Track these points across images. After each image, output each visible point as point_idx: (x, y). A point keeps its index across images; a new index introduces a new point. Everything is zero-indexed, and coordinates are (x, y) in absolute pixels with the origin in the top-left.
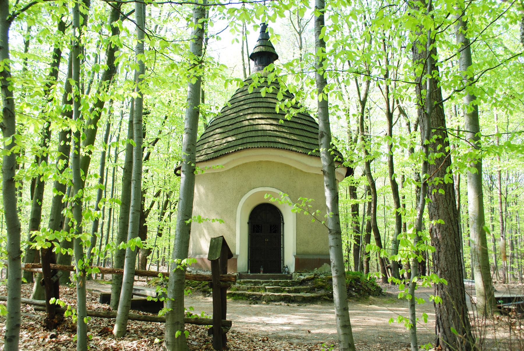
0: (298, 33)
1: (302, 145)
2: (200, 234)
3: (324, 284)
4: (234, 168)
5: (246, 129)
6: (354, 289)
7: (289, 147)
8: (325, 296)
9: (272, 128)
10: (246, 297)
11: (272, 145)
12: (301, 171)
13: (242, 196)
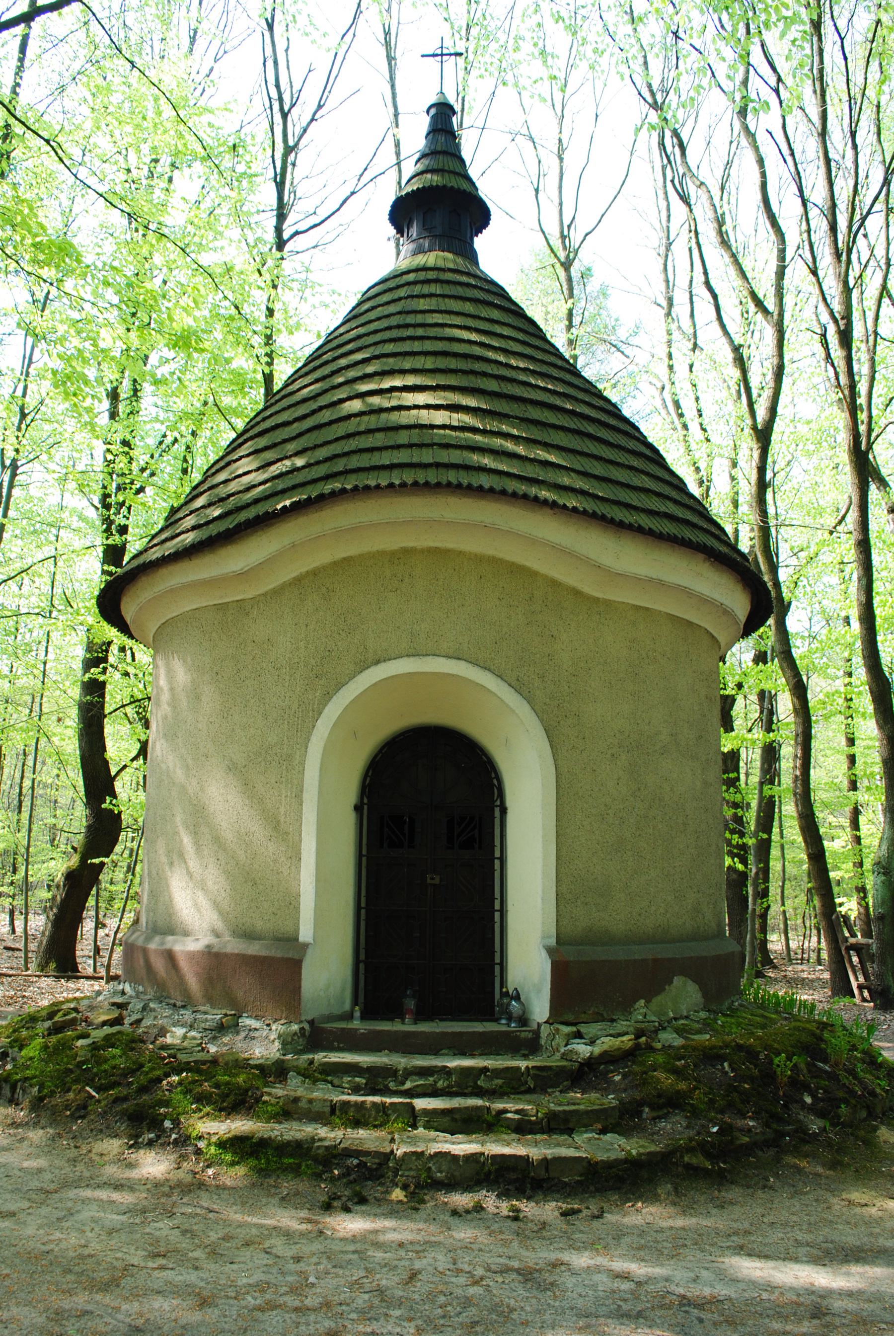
0: (562, 264)
1: (580, 483)
2: (169, 852)
3: (682, 1086)
4: (298, 581)
5: (351, 426)
6: (808, 1100)
7: (523, 488)
8: (690, 1150)
9: (456, 419)
10: (316, 1159)
11: (452, 476)
12: (577, 593)
13: (328, 696)
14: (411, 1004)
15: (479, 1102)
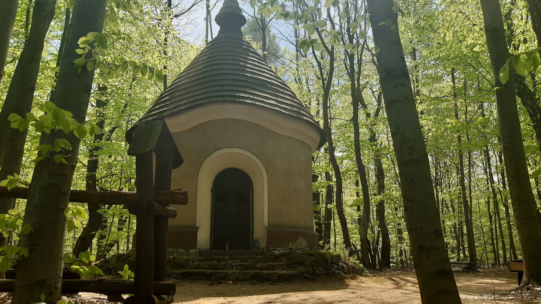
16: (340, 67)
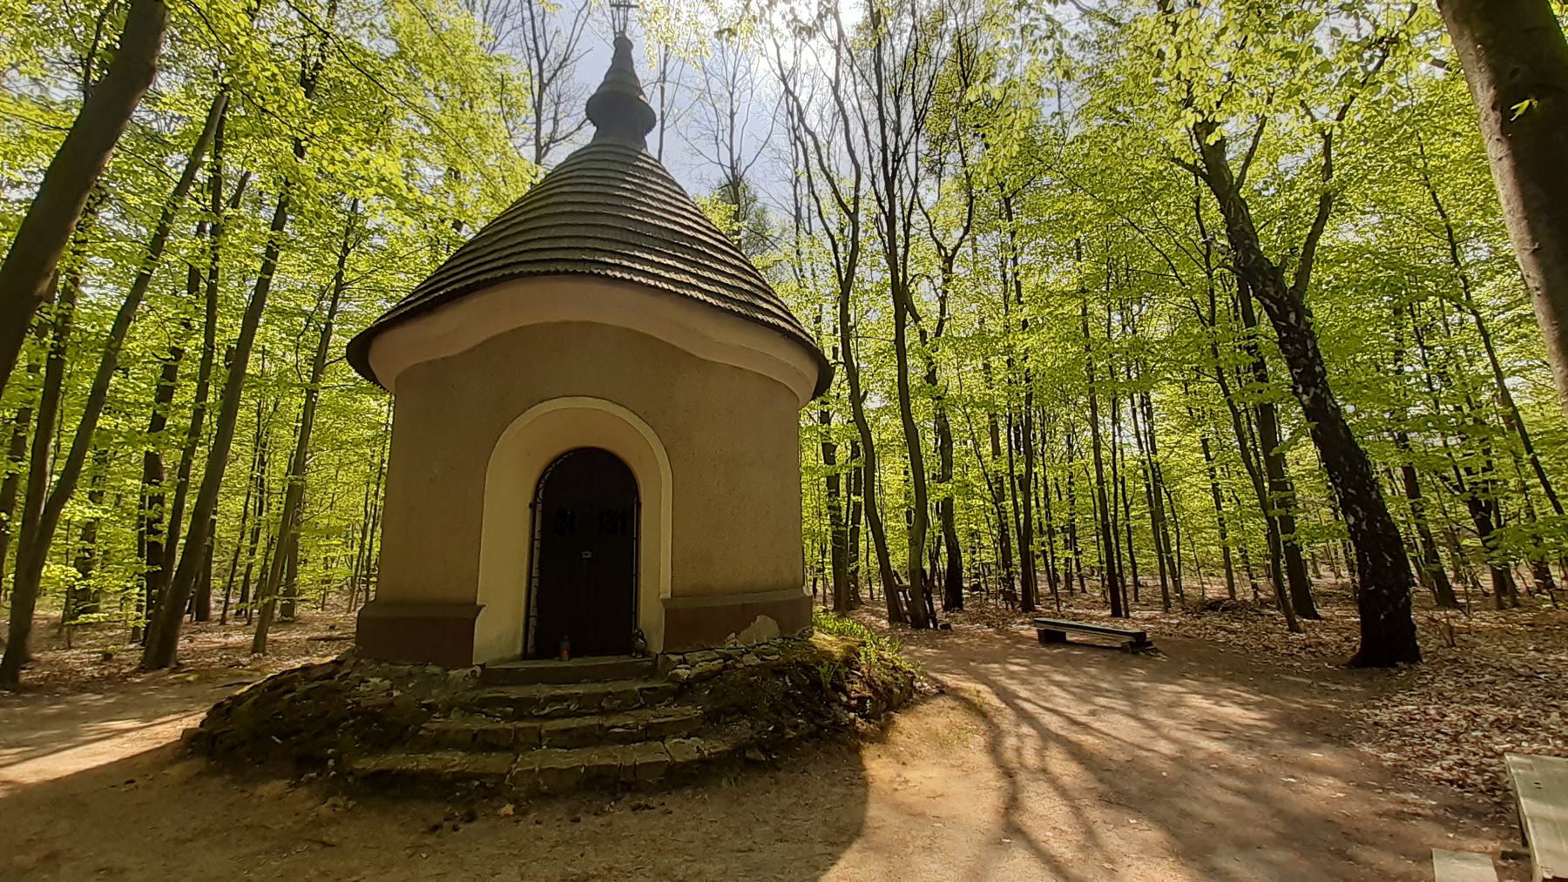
14: (565, 645)
15: (594, 721)
16: (872, 244)
